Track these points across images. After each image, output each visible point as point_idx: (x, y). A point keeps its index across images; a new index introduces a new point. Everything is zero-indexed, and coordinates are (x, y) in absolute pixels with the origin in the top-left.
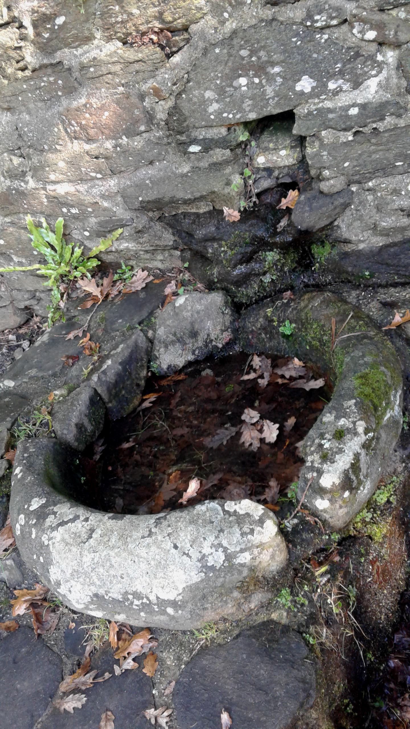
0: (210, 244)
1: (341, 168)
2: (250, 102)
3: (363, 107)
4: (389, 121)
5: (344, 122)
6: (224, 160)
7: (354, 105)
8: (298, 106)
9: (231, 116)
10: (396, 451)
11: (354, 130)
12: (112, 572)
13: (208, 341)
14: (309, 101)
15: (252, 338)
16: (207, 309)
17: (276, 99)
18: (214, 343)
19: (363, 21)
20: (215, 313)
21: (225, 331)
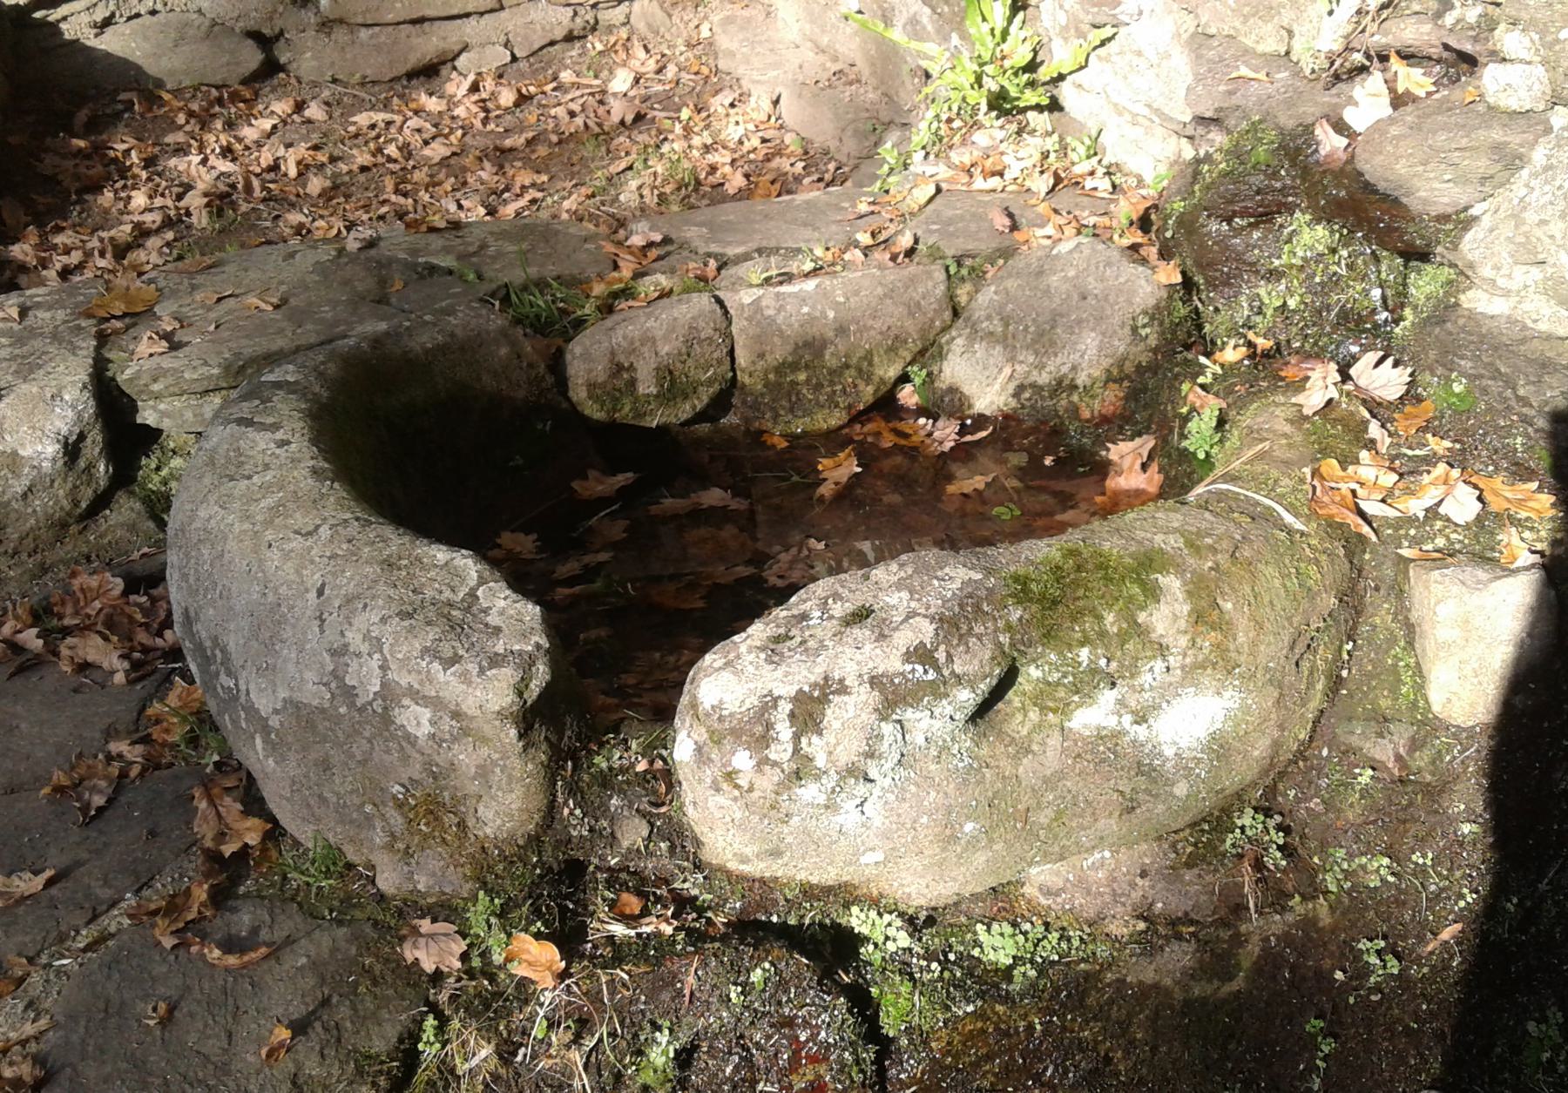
10: (1143, 874)
13: (1066, 382)
16: (1106, 298)
18: (1075, 398)
21: (1115, 381)
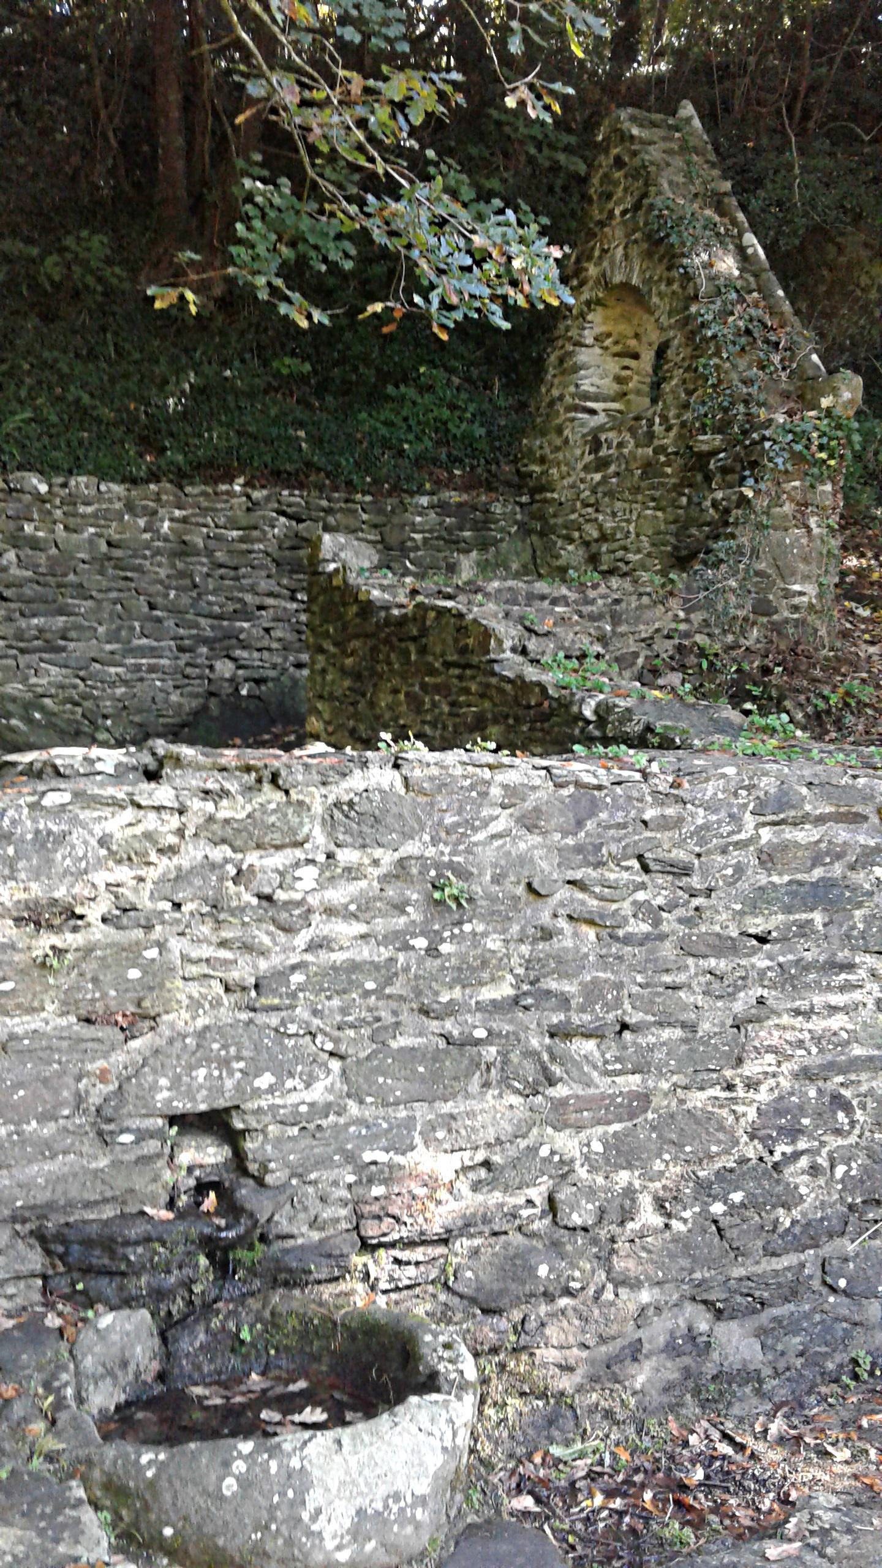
3: (312, 1105)
4: (332, 1118)
12: (378, 1471)
19: (326, 1034)
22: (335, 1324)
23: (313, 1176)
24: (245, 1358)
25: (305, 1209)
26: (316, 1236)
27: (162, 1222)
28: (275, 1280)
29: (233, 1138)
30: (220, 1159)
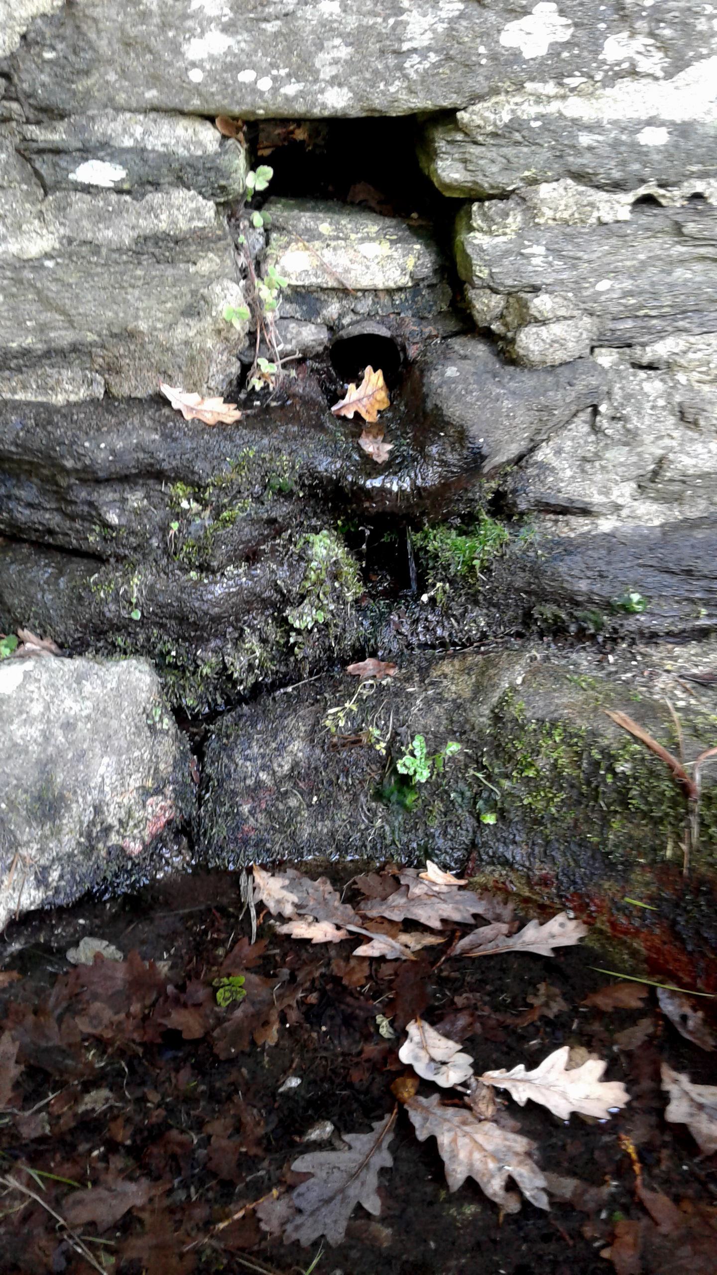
0: (111, 496)
1: (586, 293)
2: (344, 52)
3: (683, 130)
5: (623, 164)
6: (193, 231)
7: (651, 122)
8: (481, 98)
9: (265, 84)
11: (642, 191)
14: (529, 86)
15: (252, 813)
16: (104, 713)
17: (433, 57)
18: (114, 839)
20: (130, 729)
22: (685, 790)
23: (661, 349)
24: (416, 820)
25: (631, 438)
26: (651, 515)
27: (201, 428)
28: (527, 618)
29: (436, 218)
30: (395, 277)
